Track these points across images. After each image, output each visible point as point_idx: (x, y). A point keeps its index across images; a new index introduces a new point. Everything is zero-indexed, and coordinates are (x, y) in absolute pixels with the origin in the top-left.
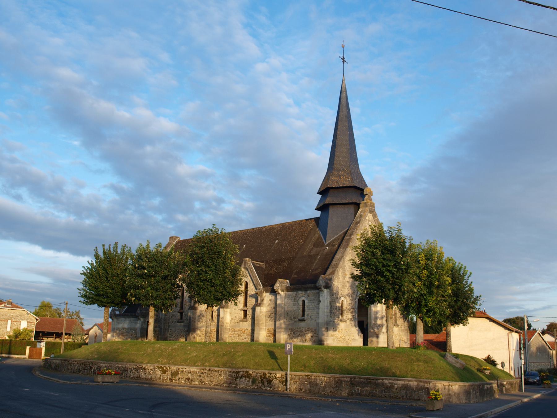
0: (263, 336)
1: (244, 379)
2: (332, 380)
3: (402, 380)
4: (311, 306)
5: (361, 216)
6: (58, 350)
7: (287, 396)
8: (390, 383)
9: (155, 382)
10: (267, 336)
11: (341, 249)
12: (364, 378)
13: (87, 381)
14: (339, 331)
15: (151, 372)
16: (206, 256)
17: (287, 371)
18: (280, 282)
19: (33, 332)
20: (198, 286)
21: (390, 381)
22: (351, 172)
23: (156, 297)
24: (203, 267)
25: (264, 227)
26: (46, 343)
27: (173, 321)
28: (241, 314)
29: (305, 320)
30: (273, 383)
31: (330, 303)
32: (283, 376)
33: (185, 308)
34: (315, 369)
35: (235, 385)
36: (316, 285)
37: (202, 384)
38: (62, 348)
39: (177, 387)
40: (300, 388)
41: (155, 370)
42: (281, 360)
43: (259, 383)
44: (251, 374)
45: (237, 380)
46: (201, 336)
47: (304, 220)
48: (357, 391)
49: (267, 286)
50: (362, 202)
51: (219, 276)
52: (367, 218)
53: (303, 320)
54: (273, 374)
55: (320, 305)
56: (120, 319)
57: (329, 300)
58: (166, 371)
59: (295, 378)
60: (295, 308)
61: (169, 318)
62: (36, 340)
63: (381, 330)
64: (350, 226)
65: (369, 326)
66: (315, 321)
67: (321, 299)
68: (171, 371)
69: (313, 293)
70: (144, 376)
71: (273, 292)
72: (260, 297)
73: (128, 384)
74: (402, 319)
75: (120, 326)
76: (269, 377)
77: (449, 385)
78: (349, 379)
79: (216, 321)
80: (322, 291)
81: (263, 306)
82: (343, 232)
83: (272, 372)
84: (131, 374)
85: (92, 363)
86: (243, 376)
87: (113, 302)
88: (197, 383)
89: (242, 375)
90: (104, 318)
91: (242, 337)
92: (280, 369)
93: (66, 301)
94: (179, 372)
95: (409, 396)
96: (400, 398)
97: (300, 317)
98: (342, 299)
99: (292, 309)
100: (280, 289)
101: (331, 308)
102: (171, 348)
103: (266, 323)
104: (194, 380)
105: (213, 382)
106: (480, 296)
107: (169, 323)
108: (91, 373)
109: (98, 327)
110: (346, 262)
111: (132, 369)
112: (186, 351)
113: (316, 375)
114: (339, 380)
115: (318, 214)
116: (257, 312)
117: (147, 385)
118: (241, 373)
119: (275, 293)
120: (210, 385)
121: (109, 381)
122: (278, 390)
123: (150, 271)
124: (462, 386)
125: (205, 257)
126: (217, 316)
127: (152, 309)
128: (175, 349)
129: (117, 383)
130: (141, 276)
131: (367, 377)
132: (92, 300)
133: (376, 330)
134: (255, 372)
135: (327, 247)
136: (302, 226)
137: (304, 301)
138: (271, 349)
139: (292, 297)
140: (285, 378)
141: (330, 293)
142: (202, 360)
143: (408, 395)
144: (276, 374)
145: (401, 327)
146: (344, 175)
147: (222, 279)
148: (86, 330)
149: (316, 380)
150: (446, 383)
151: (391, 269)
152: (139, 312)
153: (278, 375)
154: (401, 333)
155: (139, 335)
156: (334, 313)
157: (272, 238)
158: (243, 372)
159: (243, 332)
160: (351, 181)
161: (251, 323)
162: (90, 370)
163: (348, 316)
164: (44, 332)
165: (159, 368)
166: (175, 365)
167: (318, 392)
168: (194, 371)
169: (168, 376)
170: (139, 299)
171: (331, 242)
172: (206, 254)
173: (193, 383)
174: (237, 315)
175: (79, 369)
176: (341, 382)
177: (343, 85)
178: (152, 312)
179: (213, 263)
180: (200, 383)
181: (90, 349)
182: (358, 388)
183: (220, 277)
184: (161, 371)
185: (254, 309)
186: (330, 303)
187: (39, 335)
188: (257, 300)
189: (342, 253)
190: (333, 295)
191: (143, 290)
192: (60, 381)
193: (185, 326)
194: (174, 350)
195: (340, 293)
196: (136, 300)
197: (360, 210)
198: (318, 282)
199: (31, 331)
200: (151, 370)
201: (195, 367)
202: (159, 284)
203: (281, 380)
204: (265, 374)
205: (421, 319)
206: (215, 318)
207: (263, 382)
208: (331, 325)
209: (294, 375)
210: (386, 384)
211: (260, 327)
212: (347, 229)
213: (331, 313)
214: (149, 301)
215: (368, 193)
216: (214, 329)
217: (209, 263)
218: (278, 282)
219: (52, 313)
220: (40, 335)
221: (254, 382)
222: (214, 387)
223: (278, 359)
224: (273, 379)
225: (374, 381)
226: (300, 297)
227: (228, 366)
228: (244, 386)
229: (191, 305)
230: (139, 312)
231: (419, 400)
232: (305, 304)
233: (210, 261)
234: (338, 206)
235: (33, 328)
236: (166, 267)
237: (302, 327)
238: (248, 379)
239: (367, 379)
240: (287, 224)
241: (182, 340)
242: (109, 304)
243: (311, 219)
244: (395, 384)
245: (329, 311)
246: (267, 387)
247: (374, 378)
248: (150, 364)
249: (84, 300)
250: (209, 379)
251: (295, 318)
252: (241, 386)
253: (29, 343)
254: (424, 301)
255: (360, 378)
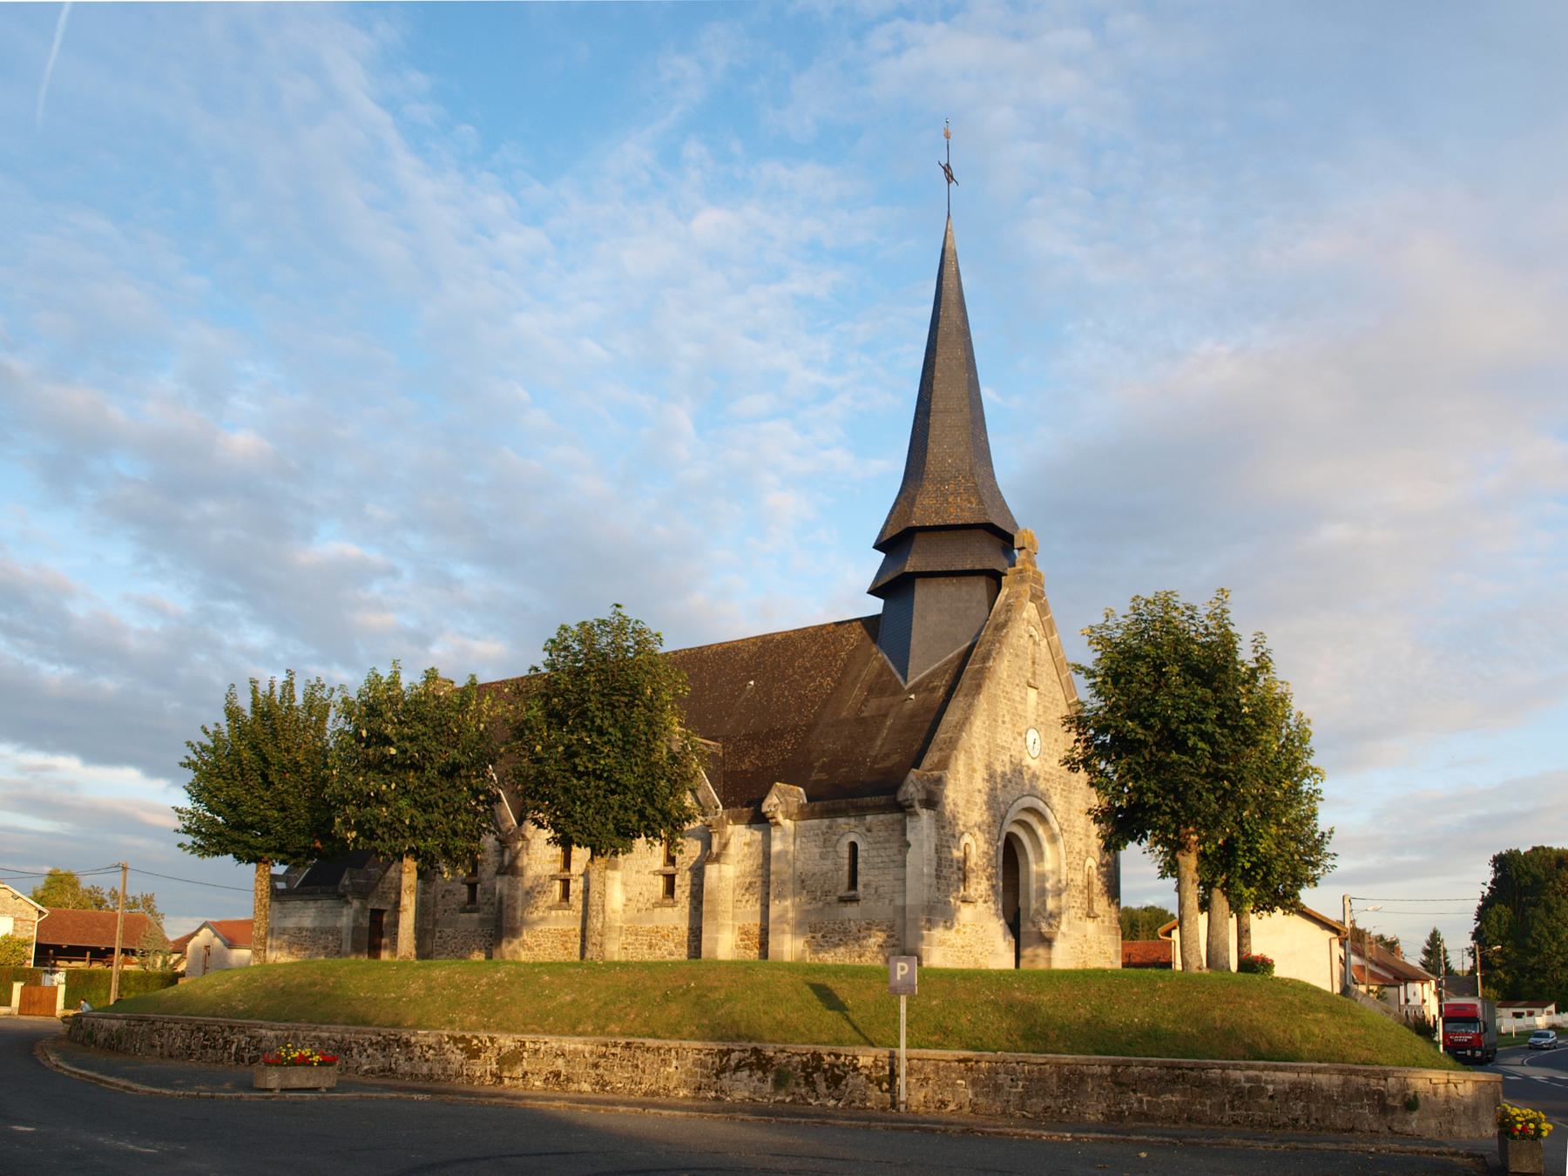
0: (725, 943)
1: (747, 1072)
2: (1051, 1074)
3: (1292, 1069)
4: (876, 860)
5: (1009, 608)
6: (103, 993)
7: (914, 1128)
8: (1248, 1079)
9: (445, 1086)
10: (737, 947)
11: (961, 699)
12: (1162, 1066)
13: (228, 1085)
14: (958, 931)
15: (428, 1055)
16: (593, 698)
17: (898, 1047)
18: (780, 790)
19: (30, 945)
20: (566, 790)
21: (1251, 1073)
22: (977, 485)
23: (425, 828)
24: (584, 734)
25: (709, 647)
26: (68, 973)
27: (447, 908)
28: (657, 886)
29: (858, 900)
30: (846, 1085)
31: (937, 849)
32: (881, 1064)
33: (484, 870)
34: (981, 1039)
35: (716, 1092)
36: (895, 799)
37: (603, 1090)
38: (114, 985)
39: (529, 1102)
40: (939, 1101)
41: (441, 1048)
42: (860, 1014)
43: (798, 1085)
44: (771, 1058)
45: (721, 1076)
46: (533, 950)
47: (830, 625)
48: (1136, 1105)
49: (734, 805)
50: (1010, 570)
51: (633, 760)
52: (1025, 615)
53: (854, 900)
54: (846, 1056)
55: (909, 857)
56: (290, 905)
57: (934, 841)
58: (479, 1050)
59: (922, 1067)
60: (828, 865)
61: (435, 897)
62: (39, 968)
63: (1058, 927)
64: (979, 634)
65: (1021, 917)
66: (891, 901)
67: (910, 837)
68: (496, 1052)
69: (882, 821)
70: (405, 1067)
71: (760, 820)
72: (717, 835)
73: (364, 1094)
74: (1106, 898)
75: (290, 923)
76: (832, 1066)
77: (1448, 1082)
78: (1107, 1070)
79: (579, 905)
80: (916, 814)
81: (728, 861)
82: (956, 652)
83: (842, 1050)
84: (363, 1062)
85: (232, 1028)
86: (744, 1066)
87: (281, 849)
88: (586, 1087)
89: (740, 1061)
90: (257, 895)
91: (660, 949)
92: (862, 1040)
93: (122, 862)
94: (525, 1054)
95: (1317, 1120)
96: (1285, 1125)
97: (843, 891)
98: (967, 839)
99: (817, 869)
100: (782, 812)
101: (939, 865)
102: (485, 980)
103: (736, 910)
104: (575, 1079)
105: (640, 1083)
106: (1331, 832)
107: (434, 915)
108: (229, 1058)
109: (212, 930)
110: (975, 735)
111: (366, 1044)
112: (538, 990)
113: (994, 1059)
114: (1072, 1073)
115: (876, 606)
116: (710, 878)
117: (426, 1097)
118: (735, 1056)
119: (765, 826)
120: (631, 1092)
121: (304, 1086)
122: (865, 1108)
123: (407, 750)
124: (1482, 1084)
125: (590, 700)
126: (584, 892)
127: (410, 865)
128: (500, 983)
129: (329, 1090)
130: (381, 766)
131: (1172, 1062)
132: (219, 842)
133: (1045, 928)
134: (783, 1051)
135: (911, 693)
136: (826, 641)
137: (853, 846)
138: (818, 979)
139: (817, 835)
140: (887, 1068)
141: (937, 821)
142: (596, 1014)
143: (1314, 1116)
144: (855, 1057)
145: (1103, 922)
146: (956, 494)
147: (641, 769)
148: (174, 942)
149: (993, 1075)
150: (1440, 1076)
151: (1209, 728)
152: (347, 883)
153: (862, 1061)
154: (1102, 938)
155: (349, 949)
156: (945, 878)
157: (736, 677)
158: (743, 1051)
159: (663, 937)
160: (979, 510)
161: (687, 910)
162: (224, 1048)
163: (979, 886)
164: (60, 946)
165: (456, 1040)
166: (508, 1030)
167: (1004, 1113)
168: (575, 1049)
169: (488, 1067)
170: (371, 836)
171: (922, 681)
172: (593, 693)
173: (574, 1087)
174: (644, 888)
175: (189, 1047)
176: (1082, 1078)
177: (948, 243)
178: (409, 873)
179: (617, 721)
180: (597, 1088)
181: (220, 985)
182: (1139, 1095)
183: (636, 764)
184: (462, 1050)
185: (698, 872)
186: (937, 851)
187: (47, 954)
188: (707, 845)
189: (962, 709)
190: (943, 827)
191: (384, 809)
192: (135, 1086)
193: (482, 921)
194: (497, 985)
195: (961, 823)
196: (361, 839)
197: (1004, 592)
198: (904, 788)
199: (25, 944)
200: (430, 1047)
201: (577, 1039)
202: (434, 789)
203: (874, 1074)
204: (817, 1057)
205: (1222, 891)
206: (577, 897)
207: (814, 1083)
208: (939, 912)
209: (919, 1060)
210: (1236, 1081)
211: (720, 921)
212: (968, 644)
213: (938, 877)
214: (400, 840)
215: (1026, 546)
216: (574, 930)
217: (602, 719)
218: (774, 791)
219: (79, 898)
220: (48, 954)
221: (779, 1083)
222: (645, 1099)
223: (847, 1010)
224: (846, 1073)
225: (1195, 1073)
226: (843, 835)
227: (686, 1031)
228: (747, 1094)
229: (503, 861)
230: (347, 883)
231: (1352, 1130)
232: (859, 853)
233: (607, 714)
234: (941, 580)
235: (31, 934)
236: (455, 739)
237: (850, 920)
238: (760, 1074)
239: (1172, 1067)
240: (779, 637)
241: (479, 956)
242: (270, 855)
243: (850, 621)
244: (1266, 1082)
245: (934, 872)
246: (826, 1096)
247: (1195, 1063)
248: (425, 1029)
249: (194, 843)
250: (626, 1075)
251: (827, 893)
252: (738, 1096)
253: (19, 975)
254: (1242, 839)
255: (1145, 1064)
